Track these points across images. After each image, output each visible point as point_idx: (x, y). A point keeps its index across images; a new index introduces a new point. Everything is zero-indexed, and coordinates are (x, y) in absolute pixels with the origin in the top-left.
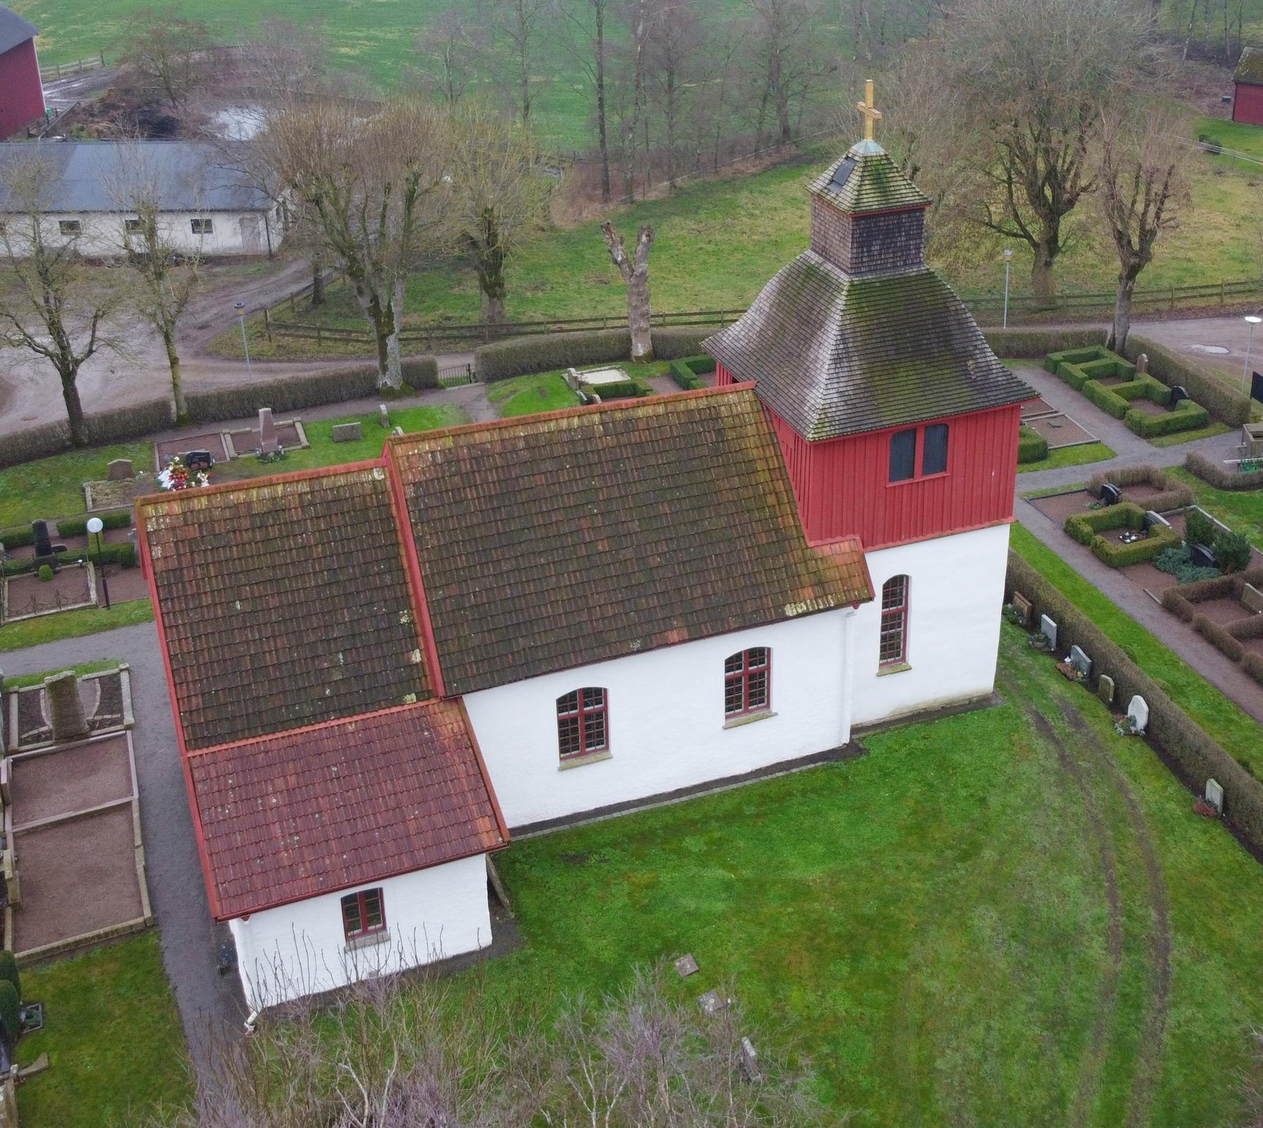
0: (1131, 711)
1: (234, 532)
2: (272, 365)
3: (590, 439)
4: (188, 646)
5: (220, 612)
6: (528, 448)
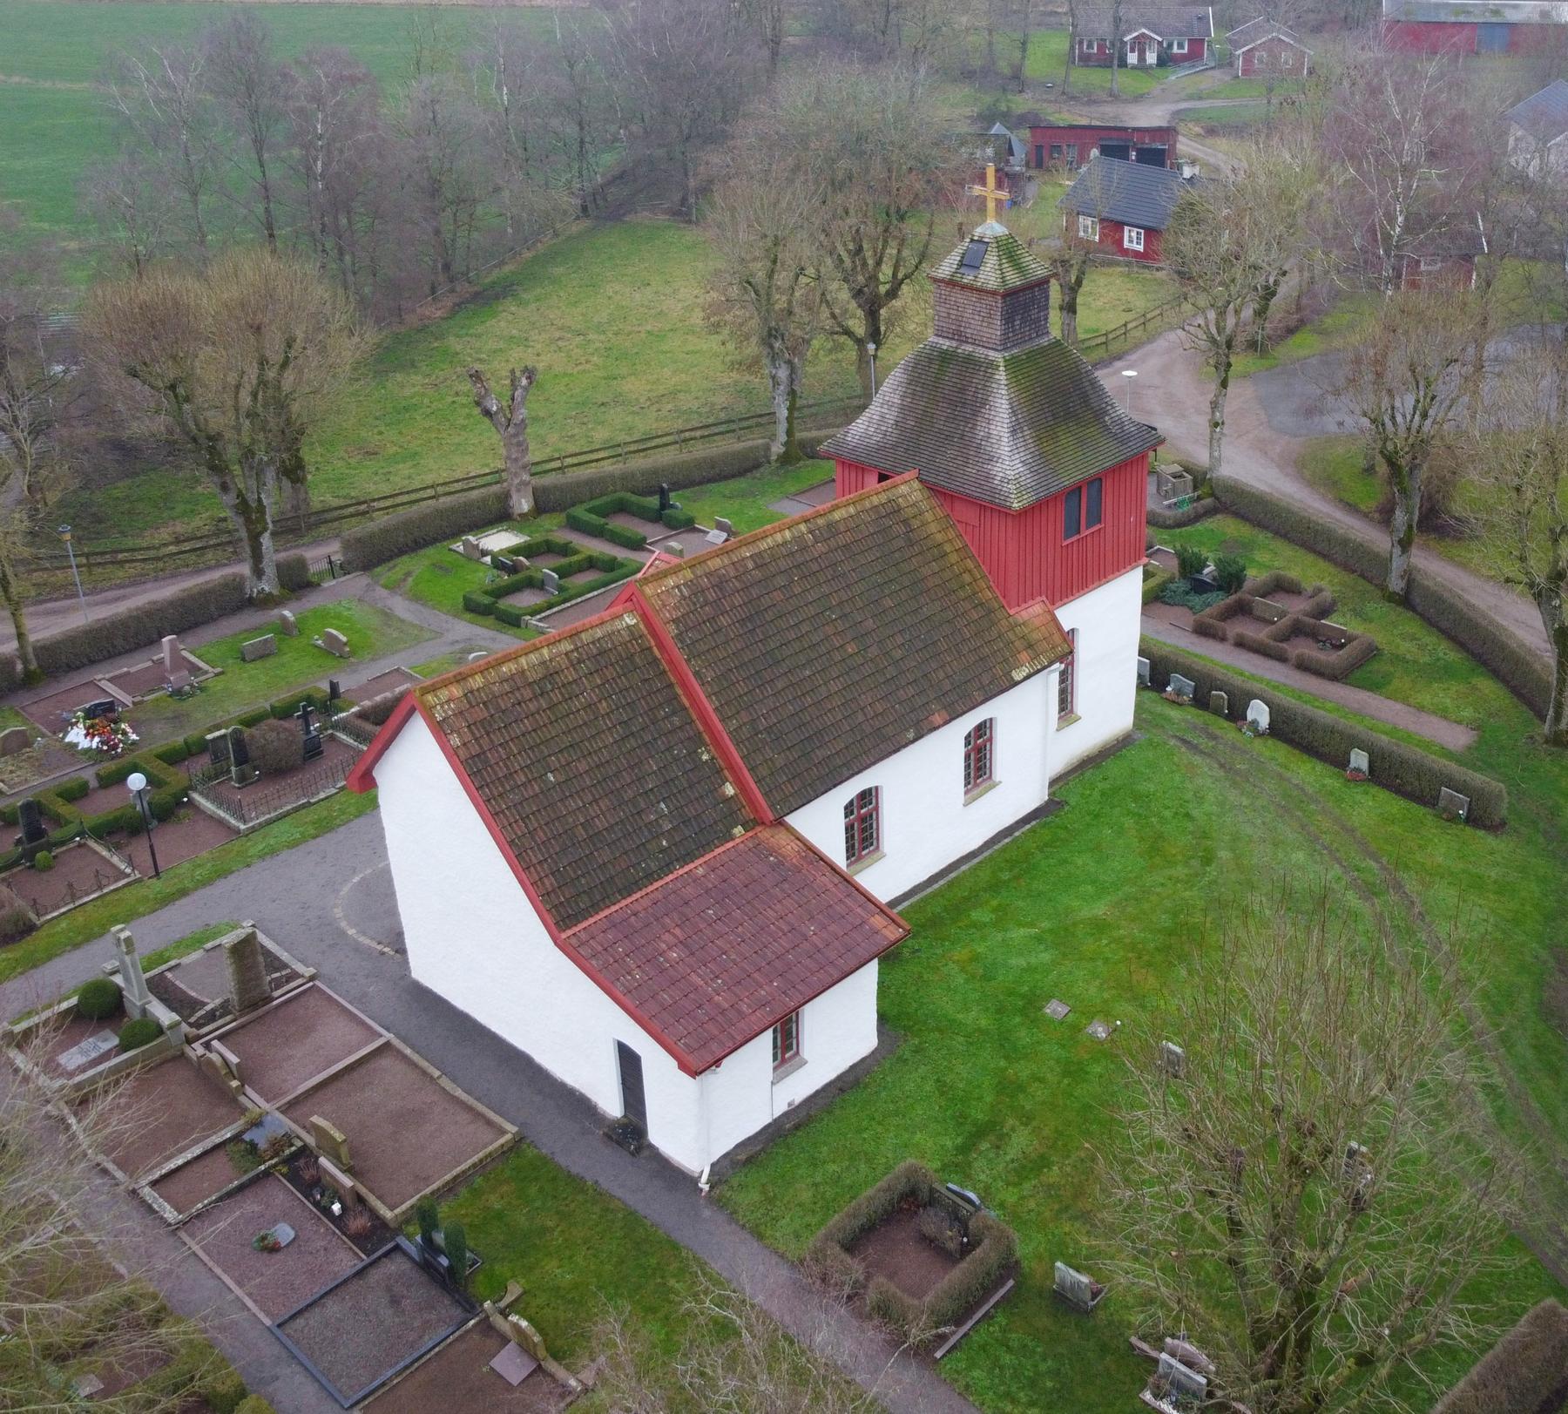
0: (1250, 715)
1: (519, 704)
2: (49, 605)
3: (804, 549)
4: (520, 829)
5: (536, 787)
6: (757, 567)
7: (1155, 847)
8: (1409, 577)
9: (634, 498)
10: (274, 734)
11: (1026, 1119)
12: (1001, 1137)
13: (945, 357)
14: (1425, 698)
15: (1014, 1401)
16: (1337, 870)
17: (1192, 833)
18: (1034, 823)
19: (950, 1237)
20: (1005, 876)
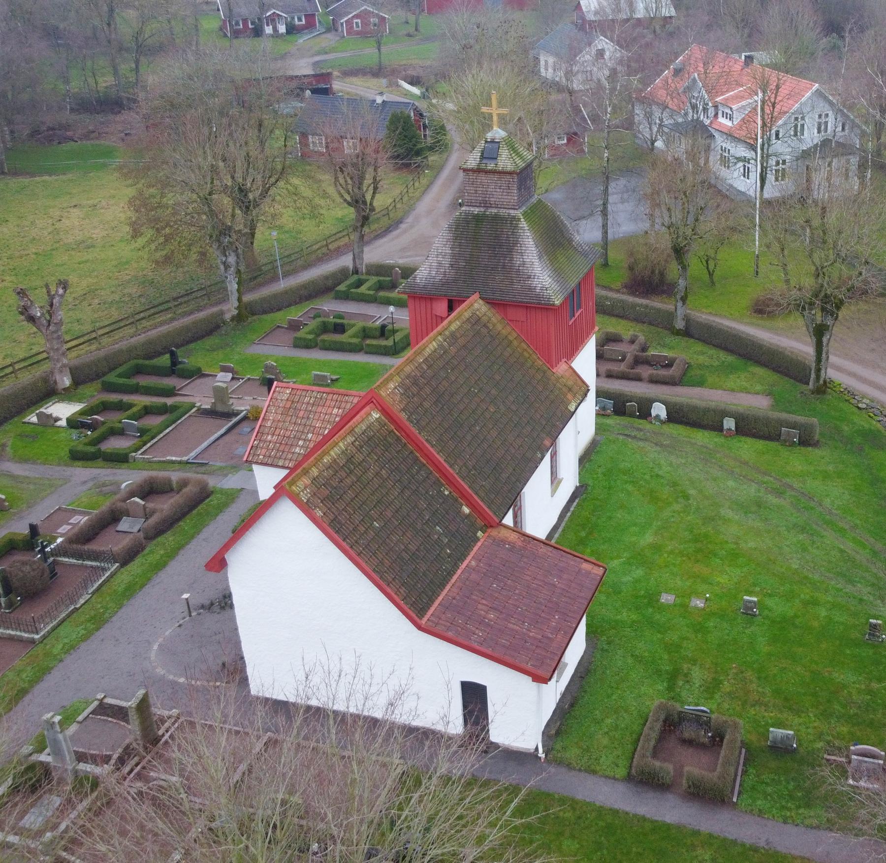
6: (430, 367)
7: (653, 497)
8: (687, 319)
9: (147, 362)
10: (28, 567)
11: (694, 662)
12: (686, 675)
13: (478, 219)
14: (730, 384)
15: (790, 809)
16: (754, 486)
17: (667, 484)
18: (577, 501)
19: (705, 736)
20: (583, 534)
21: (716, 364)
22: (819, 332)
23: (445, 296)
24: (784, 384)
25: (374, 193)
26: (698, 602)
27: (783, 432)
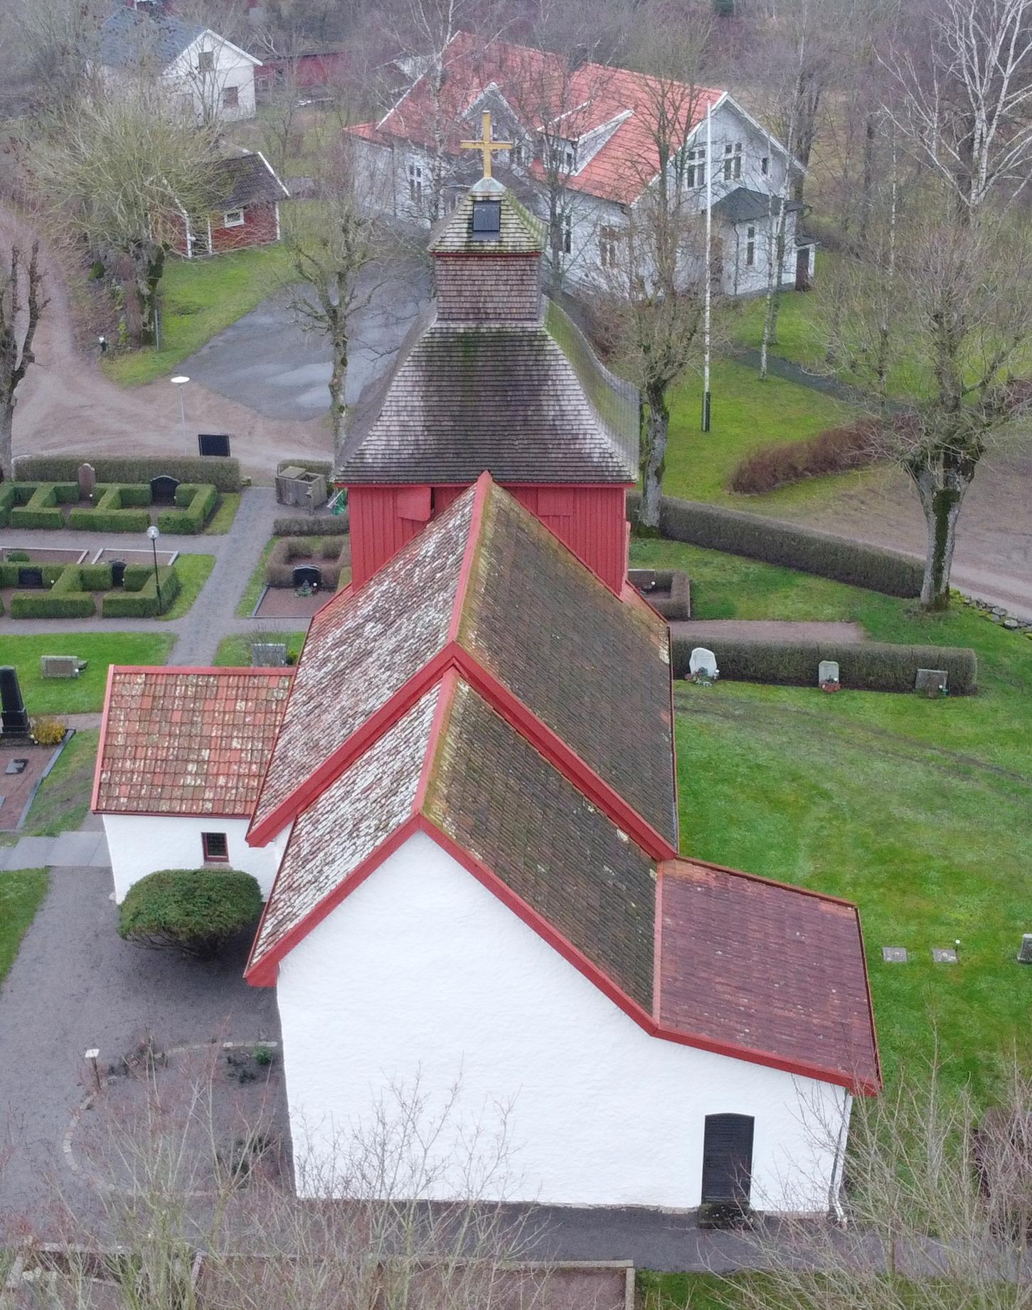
8: (663, 508)
13: (468, 342)
21: (735, 579)
22: (945, 503)
23: (427, 482)
24: (869, 601)
25: (32, 325)
26: (945, 955)
27: (919, 675)
